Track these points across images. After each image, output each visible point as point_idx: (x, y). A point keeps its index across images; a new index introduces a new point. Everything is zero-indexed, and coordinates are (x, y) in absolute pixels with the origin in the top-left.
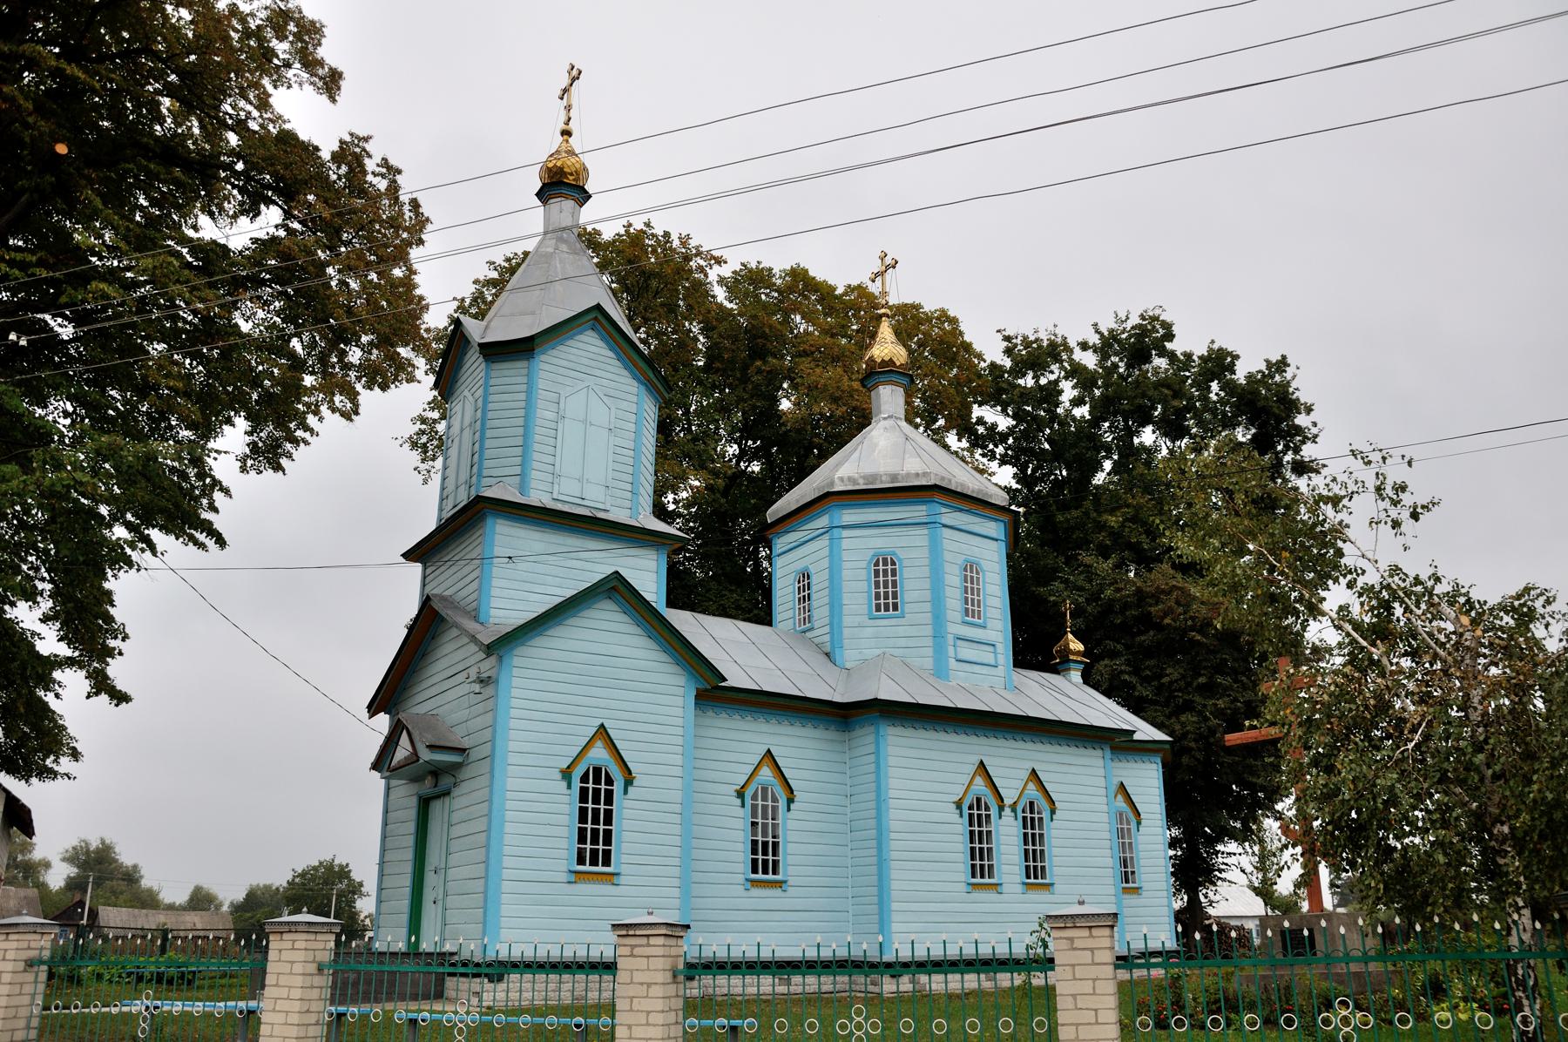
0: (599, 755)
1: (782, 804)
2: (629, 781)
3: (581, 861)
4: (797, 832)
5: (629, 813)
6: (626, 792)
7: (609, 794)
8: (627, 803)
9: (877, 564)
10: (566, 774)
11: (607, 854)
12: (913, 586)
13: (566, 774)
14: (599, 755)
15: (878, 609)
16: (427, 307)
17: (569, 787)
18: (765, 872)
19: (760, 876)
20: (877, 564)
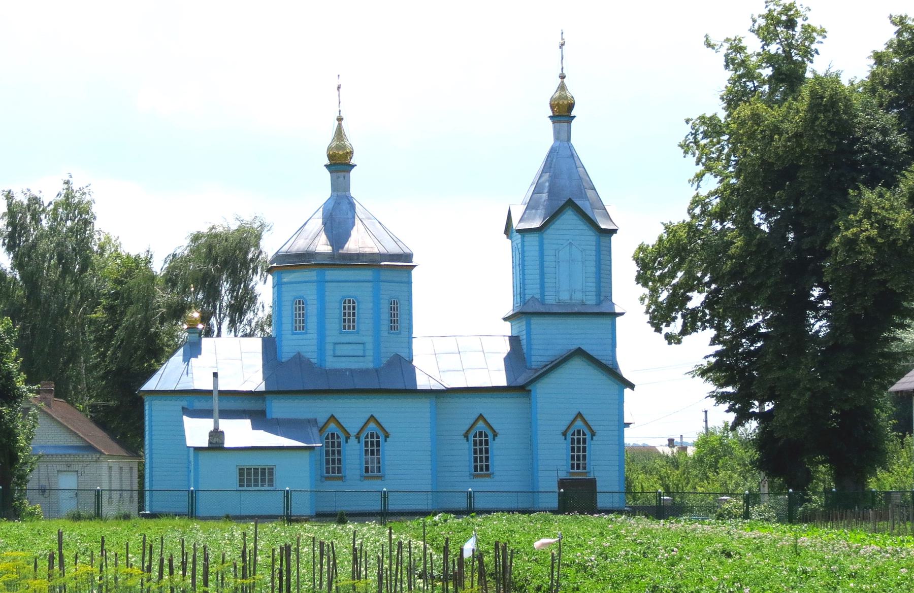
0: (579, 424)
1: (343, 439)
2: (593, 434)
3: (573, 468)
4: (464, 451)
5: (496, 447)
6: (592, 439)
7: (584, 440)
8: (592, 442)
9: (345, 303)
10: (564, 434)
11: (339, 469)
12: (365, 309)
13: (564, 434)
14: (579, 424)
15: (345, 328)
16: (75, 209)
17: (359, 442)
18: (333, 472)
19: (575, 470)
20: (345, 303)
